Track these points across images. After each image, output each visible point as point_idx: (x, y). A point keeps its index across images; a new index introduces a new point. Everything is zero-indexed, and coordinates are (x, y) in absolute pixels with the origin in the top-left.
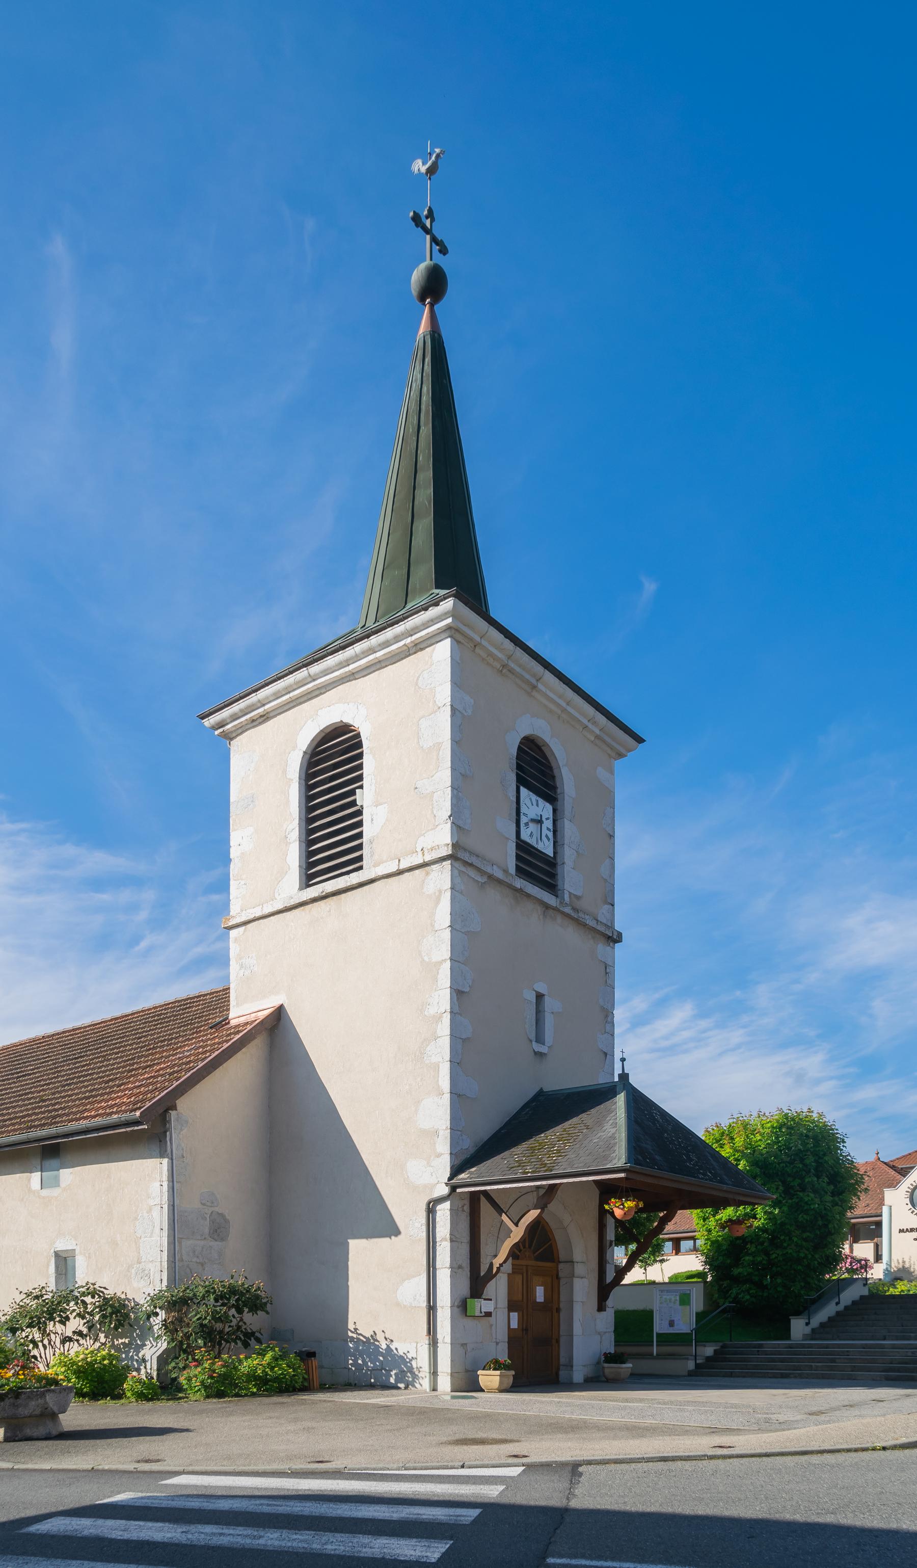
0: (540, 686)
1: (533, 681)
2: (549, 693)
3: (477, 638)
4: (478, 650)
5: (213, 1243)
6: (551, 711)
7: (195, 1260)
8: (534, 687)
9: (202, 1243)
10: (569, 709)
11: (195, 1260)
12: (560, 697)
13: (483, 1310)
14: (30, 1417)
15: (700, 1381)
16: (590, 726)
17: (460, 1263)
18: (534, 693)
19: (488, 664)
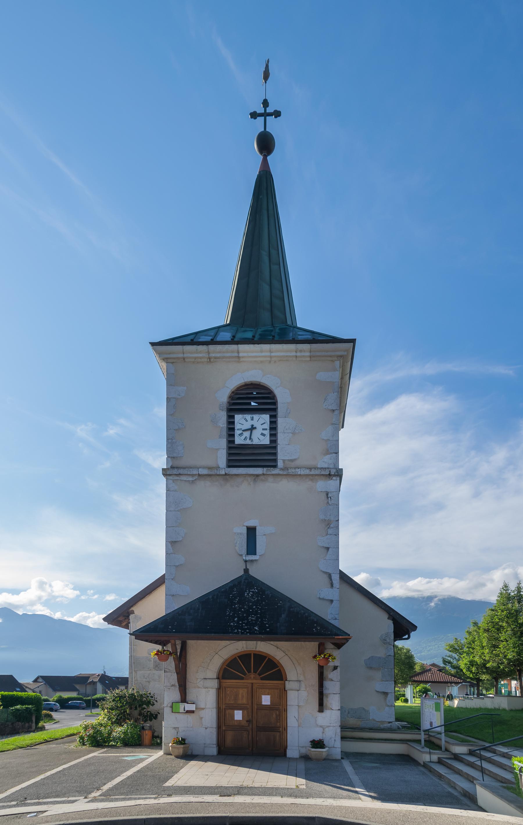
0: (241, 355)
1: (236, 354)
2: (250, 354)
3: (181, 355)
4: (186, 360)
5: (155, 672)
6: (262, 362)
7: (144, 680)
8: (239, 357)
9: (149, 672)
10: (273, 354)
11: (144, 680)
12: (262, 351)
13: (186, 709)
14: (325, 759)
15: (133, 752)
16: (299, 354)
17: (173, 683)
18: (241, 360)
19: (198, 362)
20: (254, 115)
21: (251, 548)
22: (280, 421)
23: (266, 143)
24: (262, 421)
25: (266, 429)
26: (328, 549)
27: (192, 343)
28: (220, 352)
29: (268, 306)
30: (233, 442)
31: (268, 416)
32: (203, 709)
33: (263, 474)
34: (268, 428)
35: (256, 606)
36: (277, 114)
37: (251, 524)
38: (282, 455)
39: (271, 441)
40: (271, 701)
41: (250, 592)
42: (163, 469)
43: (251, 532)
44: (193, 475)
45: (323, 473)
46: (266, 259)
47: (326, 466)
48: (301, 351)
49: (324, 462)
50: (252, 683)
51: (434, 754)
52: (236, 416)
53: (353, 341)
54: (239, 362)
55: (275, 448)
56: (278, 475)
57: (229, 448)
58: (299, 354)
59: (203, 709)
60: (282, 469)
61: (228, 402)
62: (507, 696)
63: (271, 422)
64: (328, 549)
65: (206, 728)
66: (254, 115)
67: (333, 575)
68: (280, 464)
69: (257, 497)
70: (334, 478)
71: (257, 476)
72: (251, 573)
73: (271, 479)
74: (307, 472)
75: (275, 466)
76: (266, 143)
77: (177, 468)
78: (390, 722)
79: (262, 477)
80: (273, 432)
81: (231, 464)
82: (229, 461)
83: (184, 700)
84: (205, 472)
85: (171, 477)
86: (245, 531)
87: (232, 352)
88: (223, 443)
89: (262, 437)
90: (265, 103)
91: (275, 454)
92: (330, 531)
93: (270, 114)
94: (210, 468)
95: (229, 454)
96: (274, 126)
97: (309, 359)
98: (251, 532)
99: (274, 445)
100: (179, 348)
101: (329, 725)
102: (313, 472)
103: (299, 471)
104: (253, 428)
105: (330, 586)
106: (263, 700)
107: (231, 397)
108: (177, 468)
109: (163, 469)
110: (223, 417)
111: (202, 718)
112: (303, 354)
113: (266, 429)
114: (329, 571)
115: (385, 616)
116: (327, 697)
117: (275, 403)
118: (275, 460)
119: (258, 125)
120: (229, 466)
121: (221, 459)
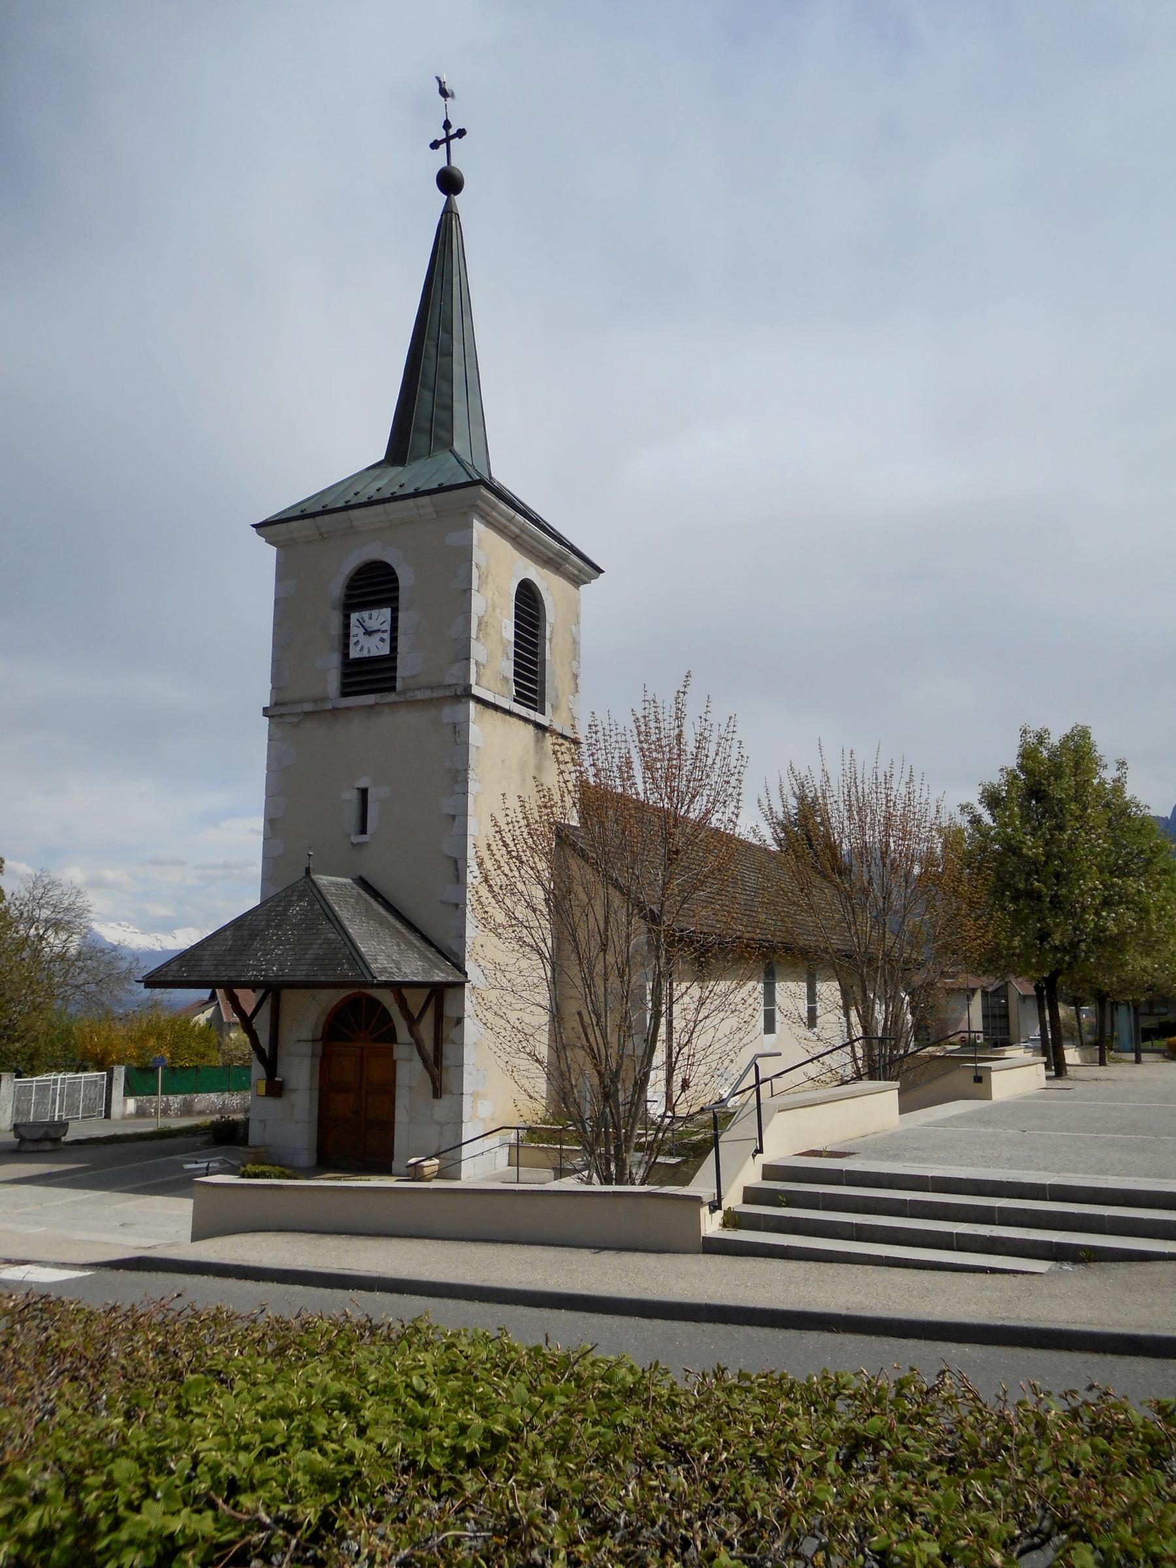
20: (435, 145)
22: (401, 615)
23: (449, 182)
24: (380, 617)
26: (454, 817)
27: (304, 516)
29: (428, 425)
37: (362, 784)
38: (403, 671)
40: (828, 979)
42: (265, 709)
43: (364, 792)
44: (297, 714)
46: (433, 351)
50: (362, 1049)
55: (396, 658)
56: (396, 703)
61: (346, 596)
62: (716, 1130)
64: (454, 817)
68: (399, 685)
71: (371, 706)
74: (427, 694)
75: (393, 689)
76: (449, 182)
81: (349, 688)
82: (344, 685)
84: (309, 707)
88: (335, 660)
90: (447, 125)
91: (395, 669)
92: (458, 788)
93: (453, 137)
94: (315, 701)
96: (463, 157)
97: (435, 516)
102: (436, 694)
103: (420, 695)
106: (792, 985)
109: (265, 709)
111: (293, 1106)
119: (438, 160)
121: (333, 682)
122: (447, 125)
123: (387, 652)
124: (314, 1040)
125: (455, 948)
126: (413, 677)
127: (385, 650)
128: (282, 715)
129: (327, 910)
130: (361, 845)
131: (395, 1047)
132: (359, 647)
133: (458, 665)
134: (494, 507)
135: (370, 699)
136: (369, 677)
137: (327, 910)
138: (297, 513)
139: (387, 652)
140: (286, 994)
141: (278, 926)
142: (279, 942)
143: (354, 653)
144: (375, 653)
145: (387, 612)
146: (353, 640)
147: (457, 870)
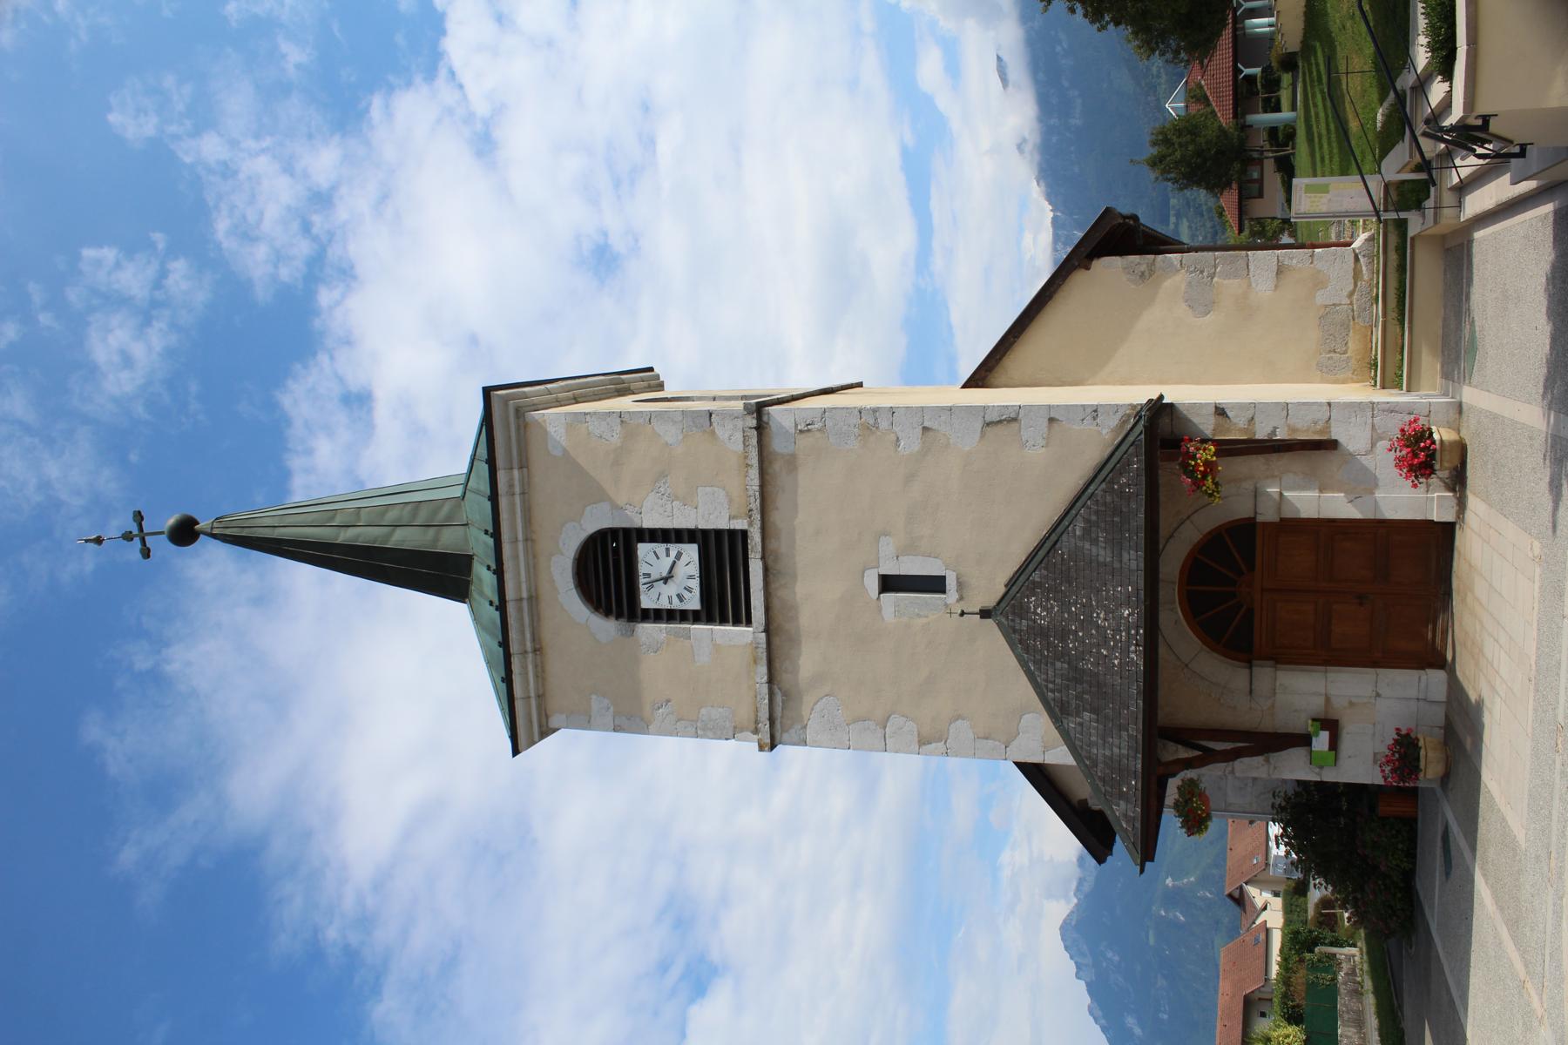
1: (525, 604)
10: (520, 537)
16: (517, 490)
20: (146, 553)
21: (934, 585)
22: (649, 522)
23: (185, 533)
24: (651, 559)
25: (668, 550)
28: (523, 633)
29: (432, 531)
30: (695, 612)
31: (640, 546)
32: (1328, 699)
33: (763, 558)
34: (664, 546)
35: (1083, 606)
36: (139, 517)
37: (873, 584)
38: (717, 519)
39: (691, 541)
41: (1035, 613)
43: (889, 584)
45: (754, 441)
46: (351, 532)
47: (739, 436)
48: (511, 486)
49: (734, 438)
51: (1439, 199)
52: (644, 605)
53: (487, 391)
54: (537, 598)
55: (705, 532)
57: (710, 620)
58: (517, 490)
59: (1328, 699)
60: (751, 524)
61: (617, 618)
63: (653, 540)
64: (925, 429)
65: (1378, 695)
66: (146, 553)
67: (988, 419)
68: (740, 524)
69: (822, 576)
70: (765, 418)
71: (766, 570)
72: (990, 601)
73: (772, 545)
75: (744, 533)
77: (757, 722)
78: (1357, 259)
79: (770, 562)
80: (673, 536)
81: (741, 616)
82: (737, 622)
83: (1305, 740)
85: (778, 735)
86: (889, 598)
87: (520, 610)
89: (684, 559)
90: (128, 537)
91: (718, 533)
93: (141, 529)
95: (723, 620)
98: (889, 584)
99: (699, 536)
100: (519, 705)
101: (1369, 427)
104: (671, 575)
105: (1014, 425)
107: (607, 613)
108: (757, 722)
110: (648, 631)
111: (1351, 704)
112: (517, 483)
113: (668, 550)
114: (979, 425)
115: (1079, 278)
116: (1293, 430)
117: (614, 532)
118: (732, 533)
119: (161, 546)
120: (749, 622)
121: (738, 639)
122: (128, 537)
123: (695, 547)
124: (1250, 668)
125: (1114, 421)
126: (730, 501)
127: (691, 552)
128: (772, 720)
129: (1042, 553)
130: (960, 585)
131: (1260, 519)
132: (686, 594)
133: (719, 431)
134: (526, 396)
135: (756, 568)
136: (728, 574)
137: (1042, 553)
138: (504, 686)
139: (695, 547)
140: (1163, 717)
141: (1064, 635)
142: (1089, 622)
143: (693, 603)
144: (694, 569)
145: (644, 550)
146: (677, 605)
147: (1000, 422)
